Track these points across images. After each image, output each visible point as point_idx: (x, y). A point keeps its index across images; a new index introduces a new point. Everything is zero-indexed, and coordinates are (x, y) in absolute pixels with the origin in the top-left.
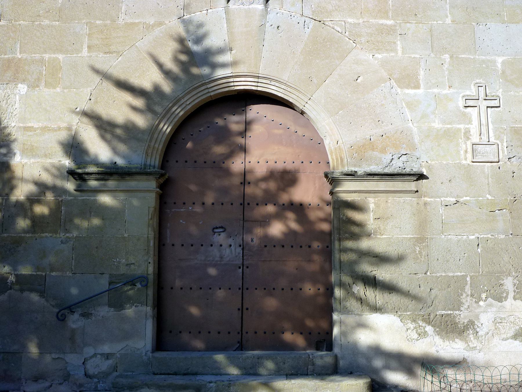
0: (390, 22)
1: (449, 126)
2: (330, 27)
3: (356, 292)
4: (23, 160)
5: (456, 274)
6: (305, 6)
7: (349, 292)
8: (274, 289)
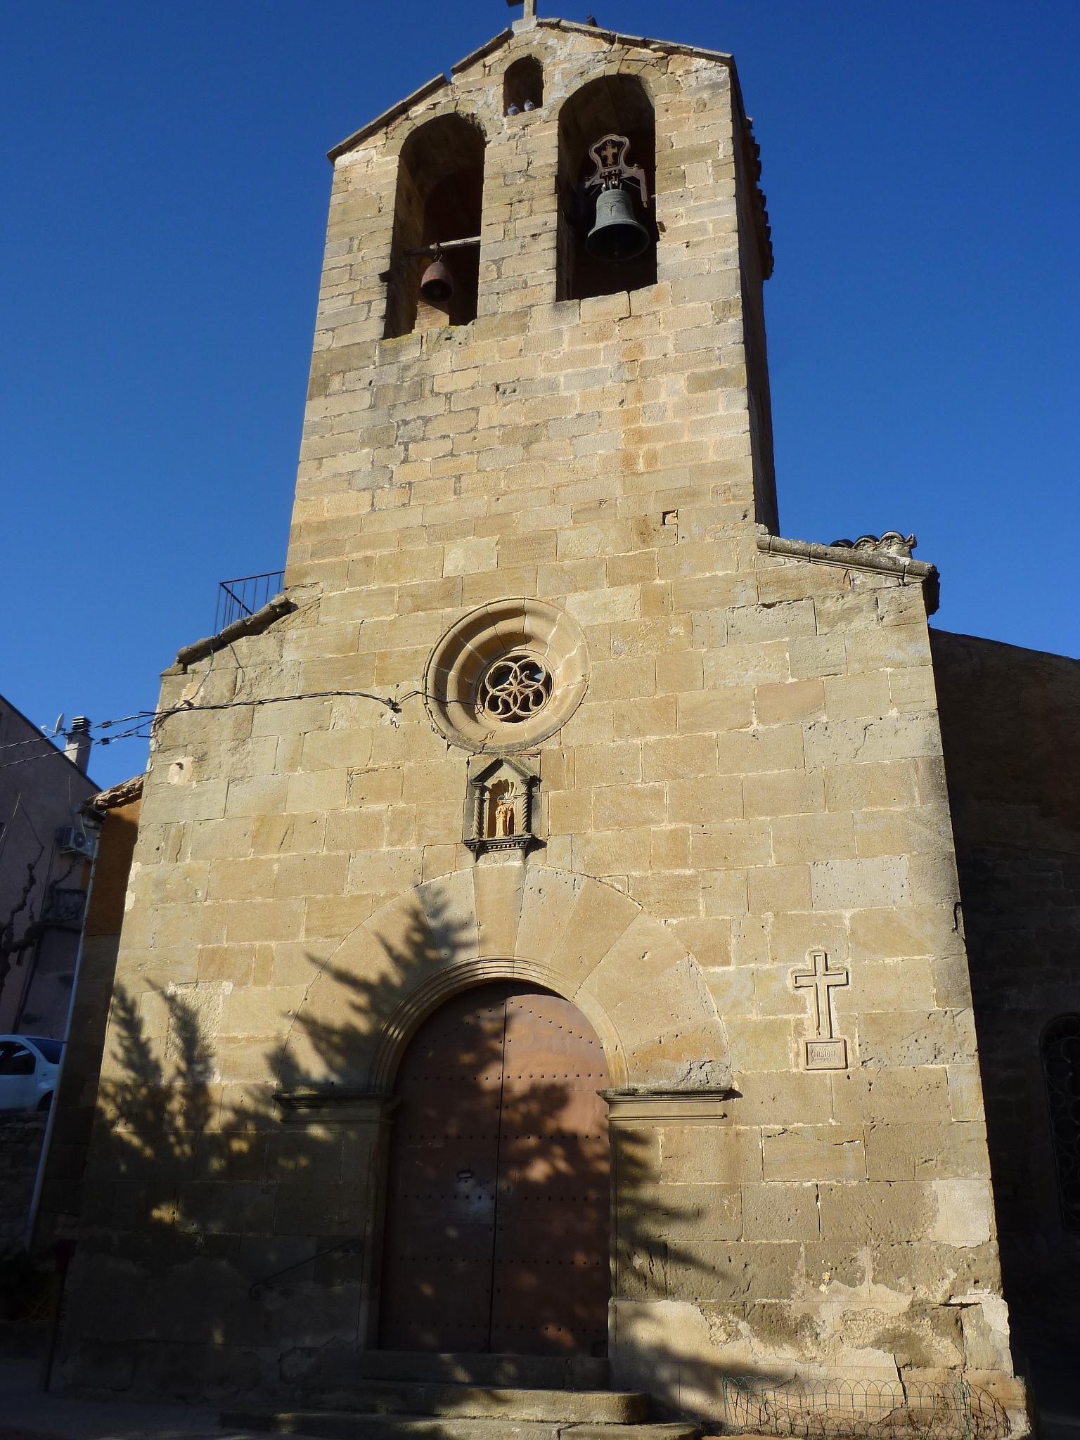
0: (688, 872)
1: (772, 1017)
2: (608, 885)
3: (637, 1267)
4: (223, 1082)
5: (783, 1242)
6: (575, 858)
7: (627, 1265)
8: (536, 1262)
